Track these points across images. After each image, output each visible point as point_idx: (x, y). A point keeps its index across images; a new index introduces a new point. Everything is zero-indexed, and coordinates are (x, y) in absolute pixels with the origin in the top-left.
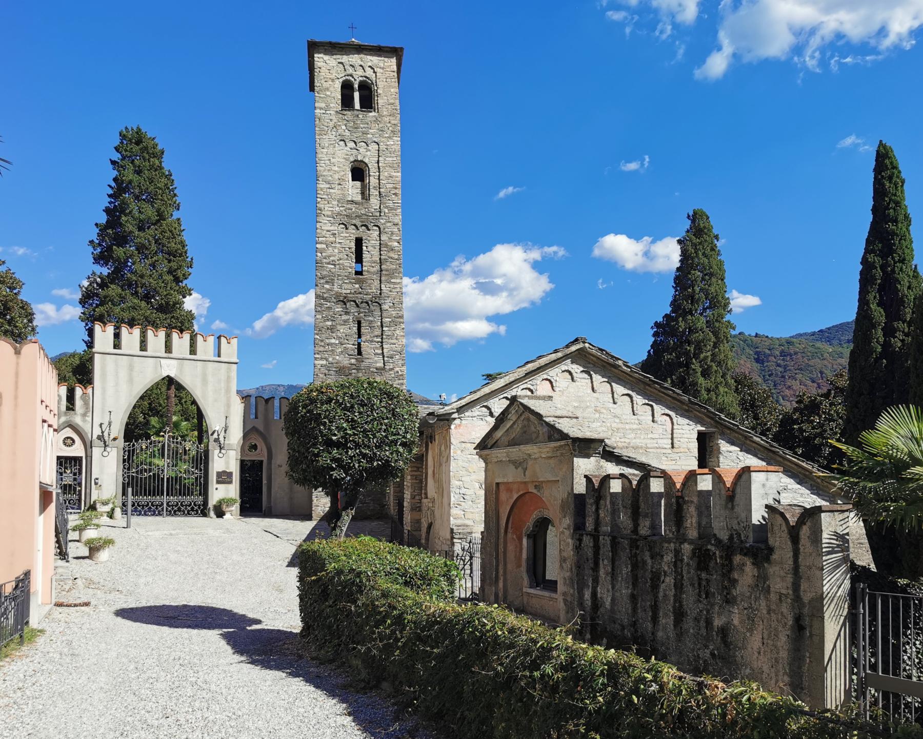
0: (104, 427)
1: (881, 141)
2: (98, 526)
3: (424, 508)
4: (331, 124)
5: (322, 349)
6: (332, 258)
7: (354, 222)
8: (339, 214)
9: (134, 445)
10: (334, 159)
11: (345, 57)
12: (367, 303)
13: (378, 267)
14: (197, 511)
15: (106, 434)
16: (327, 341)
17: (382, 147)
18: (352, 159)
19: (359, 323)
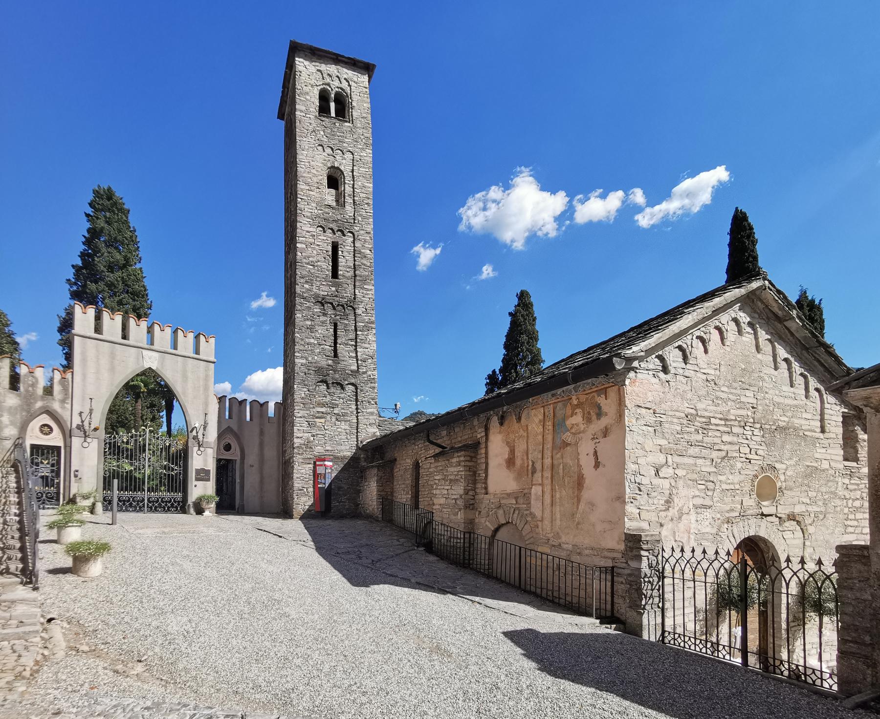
0: (84, 416)
1: (737, 208)
2: (82, 522)
4: (311, 128)
6: (311, 259)
7: (331, 226)
8: (318, 216)
9: (115, 437)
11: (323, 65)
13: (351, 273)
15: (86, 424)
17: (357, 157)
18: (329, 165)
19: (335, 325)
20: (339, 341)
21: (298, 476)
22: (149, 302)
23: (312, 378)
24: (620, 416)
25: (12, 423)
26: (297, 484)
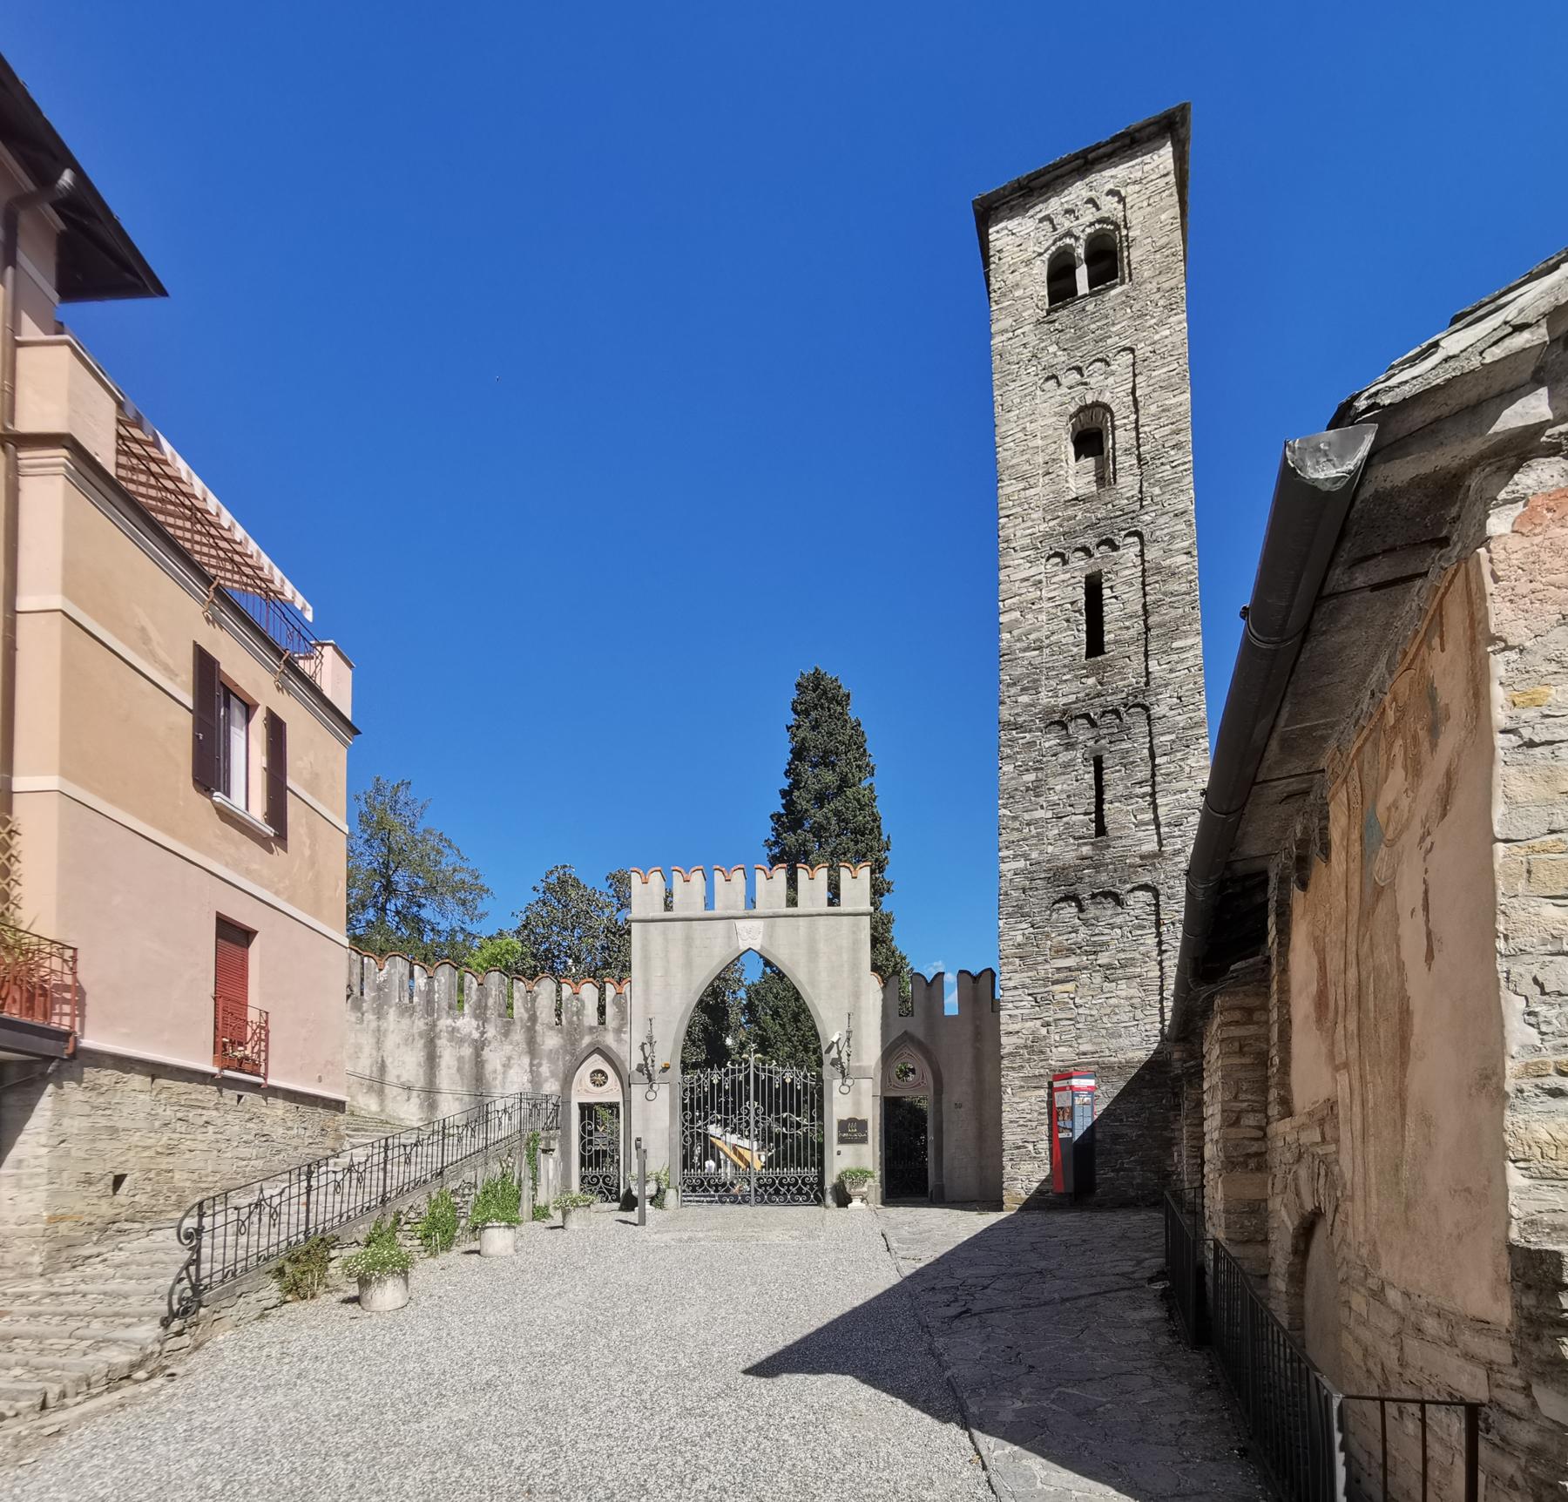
3: (1280, 1156)
5: (1015, 836)
6: (1032, 637)
7: (1081, 541)
10: (1031, 423)
12: (1116, 712)
14: (807, 1194)
16: (1027, 816)
17: (1142, 350)
18: (1072, 409)
20: (1107, 796)
21: (1013, 1117)
22: (884, 838)
23: (1042, 895)
24: (1476, 695)
25: (553, 1074)
26: (1010, 1136)
